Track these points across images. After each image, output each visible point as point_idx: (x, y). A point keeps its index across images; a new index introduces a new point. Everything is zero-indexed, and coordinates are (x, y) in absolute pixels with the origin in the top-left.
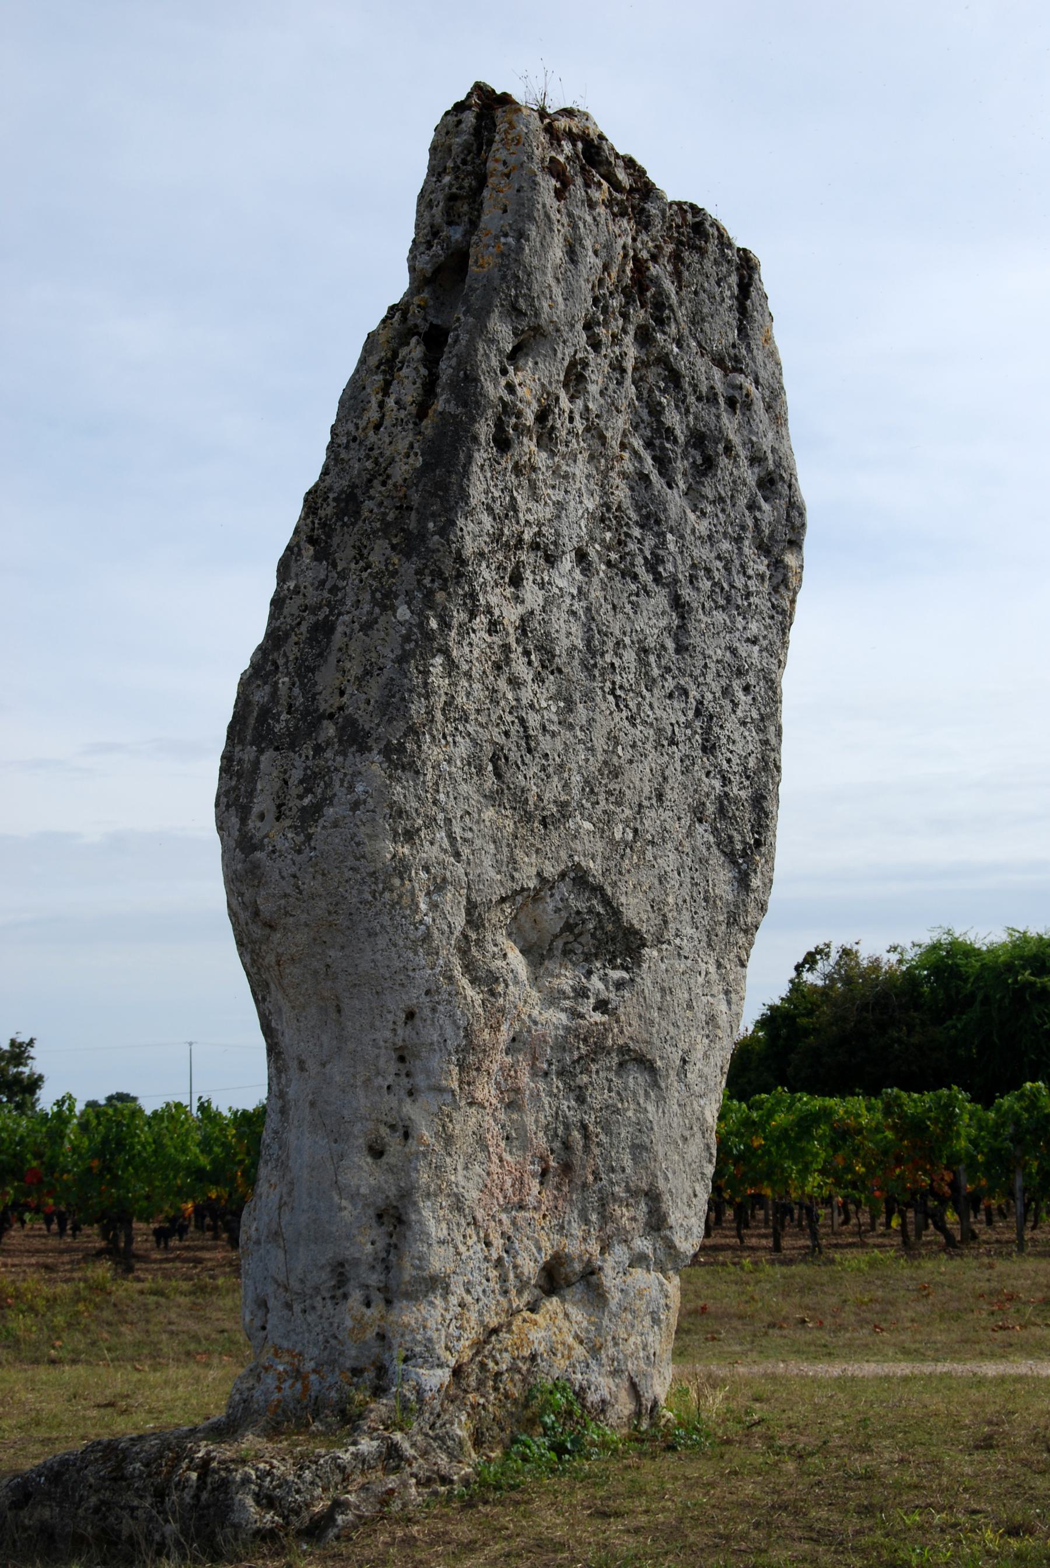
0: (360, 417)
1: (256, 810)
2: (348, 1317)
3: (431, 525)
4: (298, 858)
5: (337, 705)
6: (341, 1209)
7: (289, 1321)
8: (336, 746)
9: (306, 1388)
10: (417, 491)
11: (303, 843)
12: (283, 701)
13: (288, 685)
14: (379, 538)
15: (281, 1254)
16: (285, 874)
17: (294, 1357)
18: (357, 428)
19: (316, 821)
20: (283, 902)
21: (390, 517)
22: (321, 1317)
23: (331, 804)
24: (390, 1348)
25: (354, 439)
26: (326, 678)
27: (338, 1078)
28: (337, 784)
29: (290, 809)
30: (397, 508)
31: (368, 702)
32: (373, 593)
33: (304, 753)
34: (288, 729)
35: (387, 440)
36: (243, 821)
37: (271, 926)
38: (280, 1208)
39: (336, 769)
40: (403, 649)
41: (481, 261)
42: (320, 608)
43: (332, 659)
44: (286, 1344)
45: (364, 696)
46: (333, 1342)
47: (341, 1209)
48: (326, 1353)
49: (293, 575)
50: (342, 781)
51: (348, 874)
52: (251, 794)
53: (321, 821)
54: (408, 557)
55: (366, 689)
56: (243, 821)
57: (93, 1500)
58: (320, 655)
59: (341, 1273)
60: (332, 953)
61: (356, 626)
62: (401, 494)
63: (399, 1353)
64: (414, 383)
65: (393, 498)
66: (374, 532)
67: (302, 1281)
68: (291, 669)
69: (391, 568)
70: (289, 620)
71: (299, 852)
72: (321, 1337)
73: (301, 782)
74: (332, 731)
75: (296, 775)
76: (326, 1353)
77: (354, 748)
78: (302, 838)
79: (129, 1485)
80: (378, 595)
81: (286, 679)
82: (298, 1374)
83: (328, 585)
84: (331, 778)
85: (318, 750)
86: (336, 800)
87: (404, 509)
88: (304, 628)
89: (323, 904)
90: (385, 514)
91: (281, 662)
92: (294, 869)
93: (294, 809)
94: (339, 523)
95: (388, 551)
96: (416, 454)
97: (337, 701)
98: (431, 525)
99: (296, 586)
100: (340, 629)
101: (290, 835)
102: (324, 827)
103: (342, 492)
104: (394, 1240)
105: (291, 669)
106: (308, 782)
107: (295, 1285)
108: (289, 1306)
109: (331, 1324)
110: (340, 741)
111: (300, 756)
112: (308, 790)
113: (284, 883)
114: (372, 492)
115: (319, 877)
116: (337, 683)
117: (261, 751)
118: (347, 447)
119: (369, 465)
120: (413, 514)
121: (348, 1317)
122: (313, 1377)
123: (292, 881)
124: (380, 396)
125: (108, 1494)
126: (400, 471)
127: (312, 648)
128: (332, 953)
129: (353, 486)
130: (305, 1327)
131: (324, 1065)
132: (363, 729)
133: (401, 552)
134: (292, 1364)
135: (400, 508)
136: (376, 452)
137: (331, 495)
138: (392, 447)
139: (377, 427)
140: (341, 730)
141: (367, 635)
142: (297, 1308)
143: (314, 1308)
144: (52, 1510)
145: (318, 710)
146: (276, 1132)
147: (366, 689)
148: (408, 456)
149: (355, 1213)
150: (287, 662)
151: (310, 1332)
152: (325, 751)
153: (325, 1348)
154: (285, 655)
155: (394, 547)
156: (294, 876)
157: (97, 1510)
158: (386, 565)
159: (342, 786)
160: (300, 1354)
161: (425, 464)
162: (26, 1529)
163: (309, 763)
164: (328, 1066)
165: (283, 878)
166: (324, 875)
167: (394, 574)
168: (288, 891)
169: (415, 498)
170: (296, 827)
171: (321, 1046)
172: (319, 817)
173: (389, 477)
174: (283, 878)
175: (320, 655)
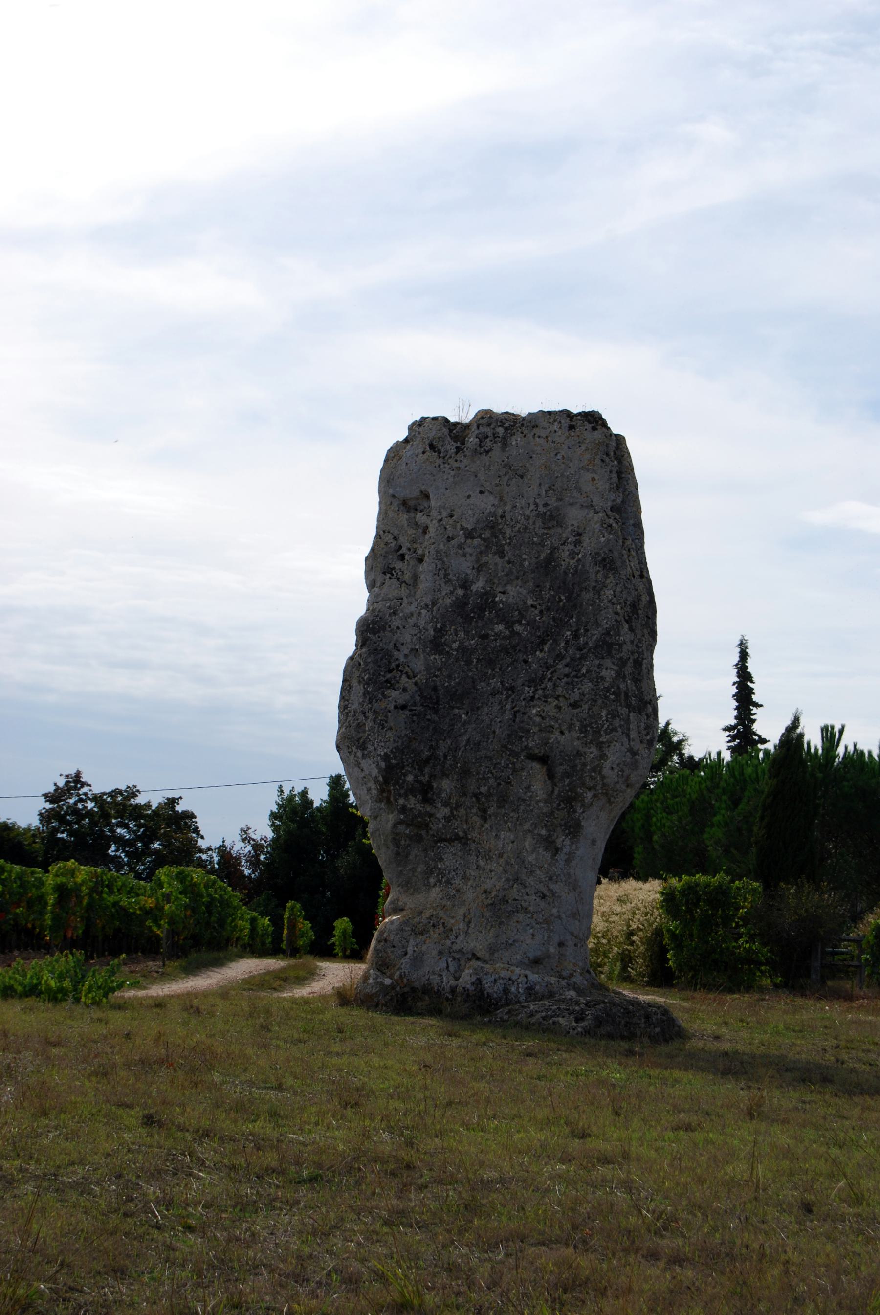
75: (643, 725)
117: (630, 712)
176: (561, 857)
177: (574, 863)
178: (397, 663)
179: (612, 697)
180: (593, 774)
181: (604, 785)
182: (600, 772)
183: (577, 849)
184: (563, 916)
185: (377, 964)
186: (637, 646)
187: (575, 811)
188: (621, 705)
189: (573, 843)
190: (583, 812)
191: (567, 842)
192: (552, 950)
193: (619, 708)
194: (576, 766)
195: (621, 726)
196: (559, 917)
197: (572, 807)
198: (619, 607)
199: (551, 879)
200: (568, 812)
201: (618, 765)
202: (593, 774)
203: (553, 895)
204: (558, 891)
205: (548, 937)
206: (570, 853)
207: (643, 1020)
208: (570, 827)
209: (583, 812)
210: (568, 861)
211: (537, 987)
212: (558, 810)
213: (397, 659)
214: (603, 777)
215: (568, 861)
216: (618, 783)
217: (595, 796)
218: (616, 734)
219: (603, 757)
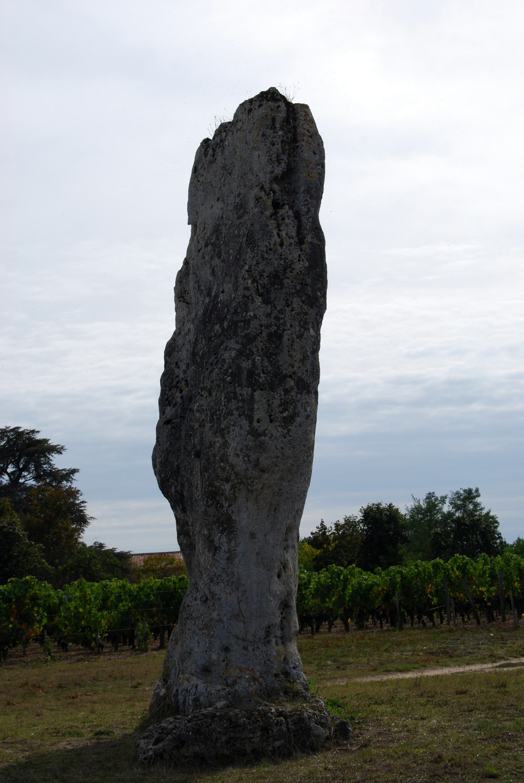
0: (270, 239)
1: (256, 418)
2: (274, 651)
3: (319, 293)
4: (285, 440)
5: (292, 371)
6: (271, 601)
7: (246, 655)
8: (296, 390)
9: (260, 684)
10: (309, 277)
11: (287, 433)
12: (259, 367)
13: (260, 361)
14: (295, 297)
15: (241, 625)
16: (278, 447)
17: (250, 671)
18: (270, 244)
19: (292, 423)
20: (275, 460)
21: (298, 287)
22: (262, 652)
23: (298, 416)
24: (288, 664)
25: (271, 250)
26: (283, 359)
27: (272, 541)
28: (300, 407)
29: (277, 418)
30: (300, 284)
31: (307, 371)
32: (299, 322)
33: (279, 392)
34: (268, 381)
35: (289, 252)
36: (251, 422)
37: (263, 471)
38: (239, 603)
39: (298, 400)
40: (313, 348)
41: (311, 175)
42: (271, 326)
43: (285, 350)
44: (244, 666)
45: (305, 369)
46: (268, 662)
47: (271, 601)
48: (265, 668)
49: (251, 309)
50: (302, 406)
51: (303, 448)
52: (252, 410)
53: (294, 424)
54: (312, 308)
55: (305, 365)
56: (251, 422)
57: (224, 738)
58: (277, 347)
59: (268, 631)
60: (284, 484)
61: (294, 336)
62: (301, 278)
63: (291, 666)
64: (294, 227)
65: (298, 279)
66: (292, 294)
67: (254, 636)
68: (261, 353)
69: (304, 311)
70: (255, 330)
71: (285, 437)
72: (263, 661)
73: (280, 405)
74: (292, 383)
75: (277, 402)
76: (265, 668)
77: (305, 392)
78: (286, 431)
79: (244, 729)
80: (302, 323)
81: (259, 358)
82: (254, 679)
83: (273, 316)
84: (296, 404)
85: (286, 391)
86: (300, 414)
87: (304, 284)
88: (264, 334)
89: (291, 461)
90: (295, 286)
91: (254, 349)
92: (282, 445)
93: (279, 419)
94: (272, 288)
95: (301, 303)
96: (303, 260)
97: (291, 370)
98: (319, 293)
99: (254, 315)
100: (286, 337)
101: (280, 430)
102: (296, 427)
103: (271, 273)
104: (284, 615)
105: (261, 353)
106: (284, 405)
107: (250, 637)
108: (245, 648)
109: (267, 654)
110: (298, 388)
111: (277, 393)
112: (285, 410)
113: (277, 451)
114: (287, 275)
115: (292, 449)
116: (290, 361)
117: (254, 391)
118: (267, 252)
119: (282, 262)
120: (309, 288)
121: (274, 651)
122: (261, 679)
123: (281, 450)
124: (277, 230)
125: (232, 734)
126: (299, 267)
127: (271, 344)
128: (284, 484)
129: (277, 272)
130: (254, 657)
131: (265, 536)
132: (307, 383)
133: (307, 304)
134: (251, 674)
135: (302, 284)
136: (283, 257)
137: (265, 275)
138: (291, 256)
139: (282, 245)
140: (297, 383)
141: (301, 341)
142: (250, 648)
143: (258, 648)
144: (199, 747)
145: (282, 373)
146: (224, 569)
147: (305, 365)
148: (299, 260)
149: (275, 603)
150: (258, 350)
151: (256, 659)
152: (290, 392)
153: (265, 665)
154: (256, 346)
155: (303, 302)
156: (282, 448)
157: (228, 742)
158: (301, 309)
159: (302, 408)
160: (252, 670)
161: (310, 265)
162: (186, 757)
163: (283, 397)
164: (267, 536)
165: (277, 449)
166: (293, 448)
167: (306, 314)
168: (279, 455)
169: (309, 281)
170: (283, 426)
171: (265, 527)
172: (294, 422)
173: (293, 269)
174: (277, 449)
175: (277, 347)
176: (222, 555)
177: (236, 561)
178: (177, 379)
179: (229, 379)
180: (222, 464)
181: (236, 474)
182: (228, 462)
183: (237, 545)
184: (225, 619)
185: (164, 674)
186: (277, 318)
187: (222, 507)
188: (240, 385)
189: (230, 540)
190: (230, 506)
191: (224, 539)
192: (214, 657)
193: (238, 389)
194: (209, 458)
195: (237, 409)
196: (220, 621)
197: (218, 503)
198: (250, 281)
199: (212, 581)
200: (217, 508)
201: (241, 450)
202: (222, 464)
203: (213, 597)
204: (218, 593)
205: (209, 644)
206: (229, 551)
207: (259, 733)
208: (222, 523)
209: (230, 506)
210: (230, 559)
211: (202, 698)
212: (208, 507)
213: (178, 376)
214: (232, 466)
215: (230, 559)
216: (247, 469)
217: (233, 487)
218: (232, 418)
219: (225, 444)
